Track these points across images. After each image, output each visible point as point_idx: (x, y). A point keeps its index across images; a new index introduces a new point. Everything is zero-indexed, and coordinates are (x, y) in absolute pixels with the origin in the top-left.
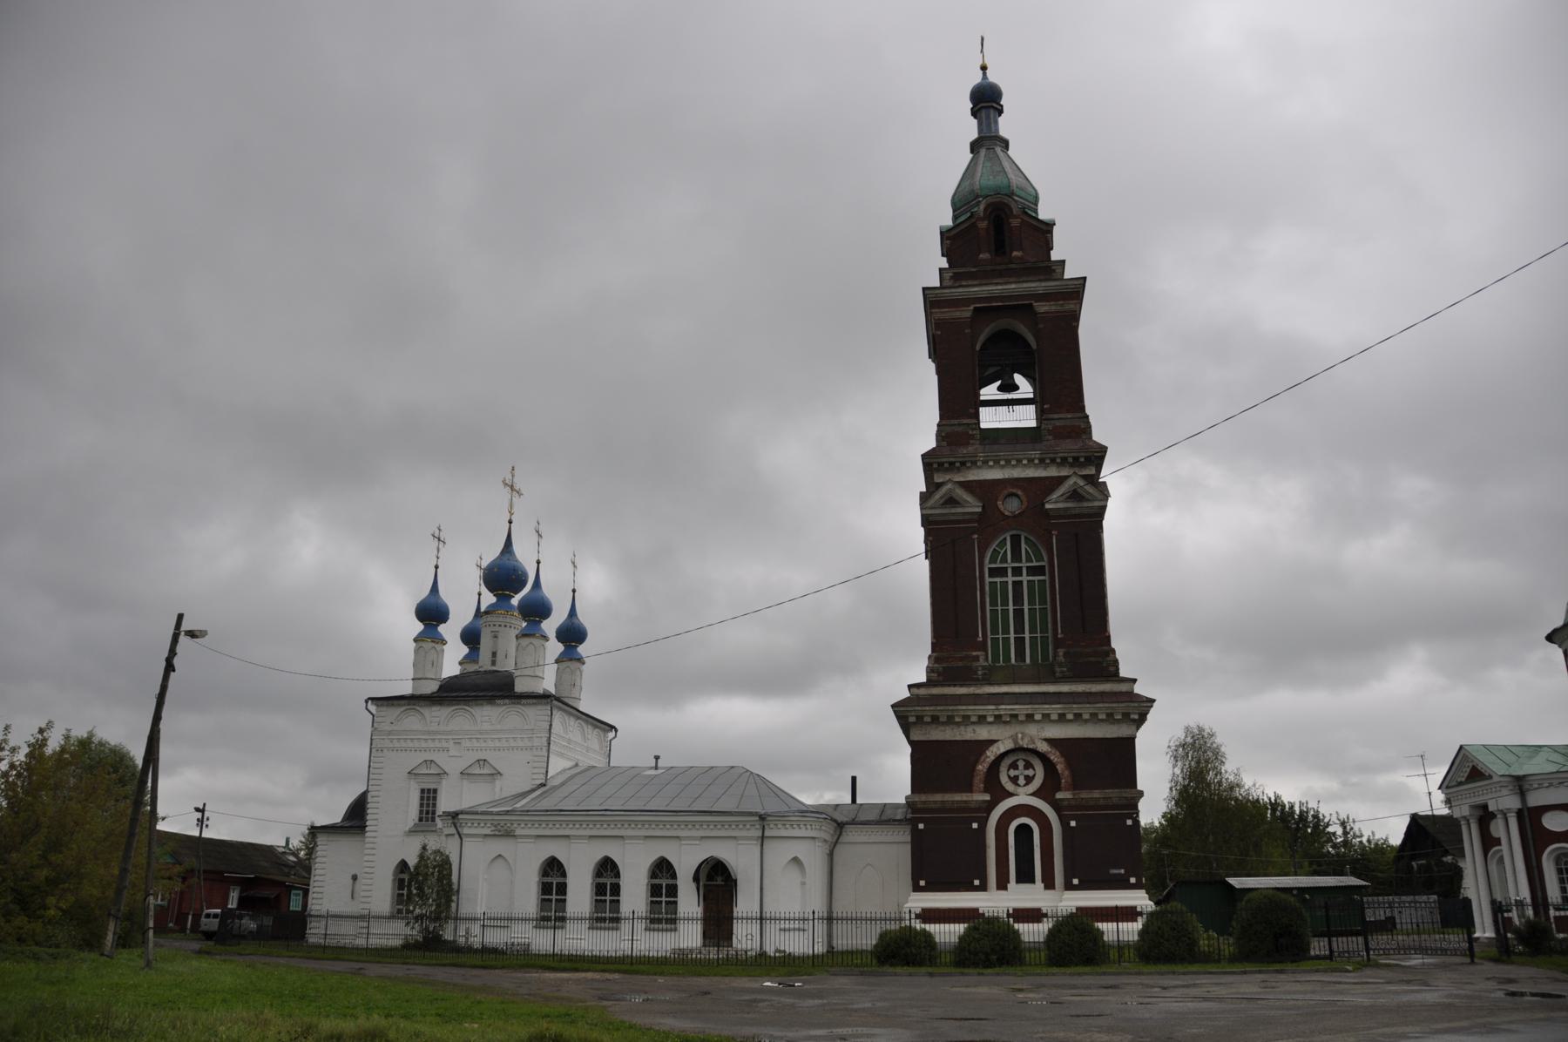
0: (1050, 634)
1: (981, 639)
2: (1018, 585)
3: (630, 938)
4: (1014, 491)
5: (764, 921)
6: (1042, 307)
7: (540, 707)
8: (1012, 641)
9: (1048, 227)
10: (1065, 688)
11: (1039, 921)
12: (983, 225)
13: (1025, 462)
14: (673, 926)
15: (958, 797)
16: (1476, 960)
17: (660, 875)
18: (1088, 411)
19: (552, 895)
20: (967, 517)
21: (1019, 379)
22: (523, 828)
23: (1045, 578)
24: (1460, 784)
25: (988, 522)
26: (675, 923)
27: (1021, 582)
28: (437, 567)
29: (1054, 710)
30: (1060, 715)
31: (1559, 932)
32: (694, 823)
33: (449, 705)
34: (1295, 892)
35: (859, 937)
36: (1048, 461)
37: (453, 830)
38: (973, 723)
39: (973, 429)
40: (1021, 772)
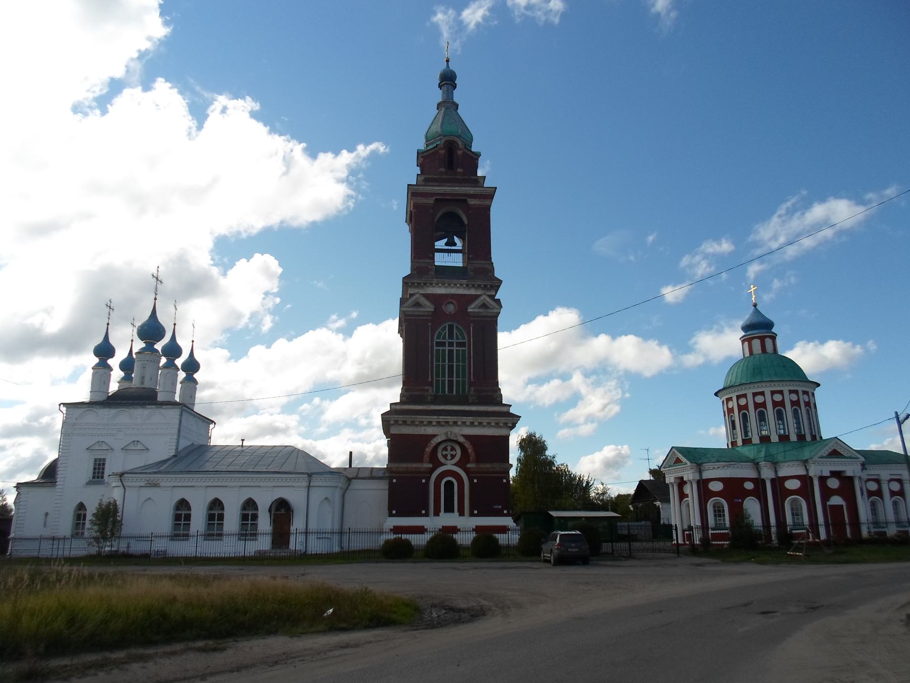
2: (451, 352)
3: (195, 545)
4: (452, 301)
5: (308, 534)
8: (447, 381)
12: (443, 152)
13: (458, 285)
14: (254, 538)
15: (415, 465)
16: (680, 555)
17: (248, 508)
19: (181, 521)
20: (426, 314)
21: (456, 239)
22: (216, 482)
23: (466, 349)
24: (670, 466)
25: (438, 316)
26: (256, 536)
27: (453, 350)
28: (108, 324)
29: (469, 420)
30: (504, 423)
31: (687, 541)
33: (115, 408)
34: (583, 519)
36: (470, 286)
37: (120, 484)
38: (425, 425)
39: (431, 266)
40: (449, 453)
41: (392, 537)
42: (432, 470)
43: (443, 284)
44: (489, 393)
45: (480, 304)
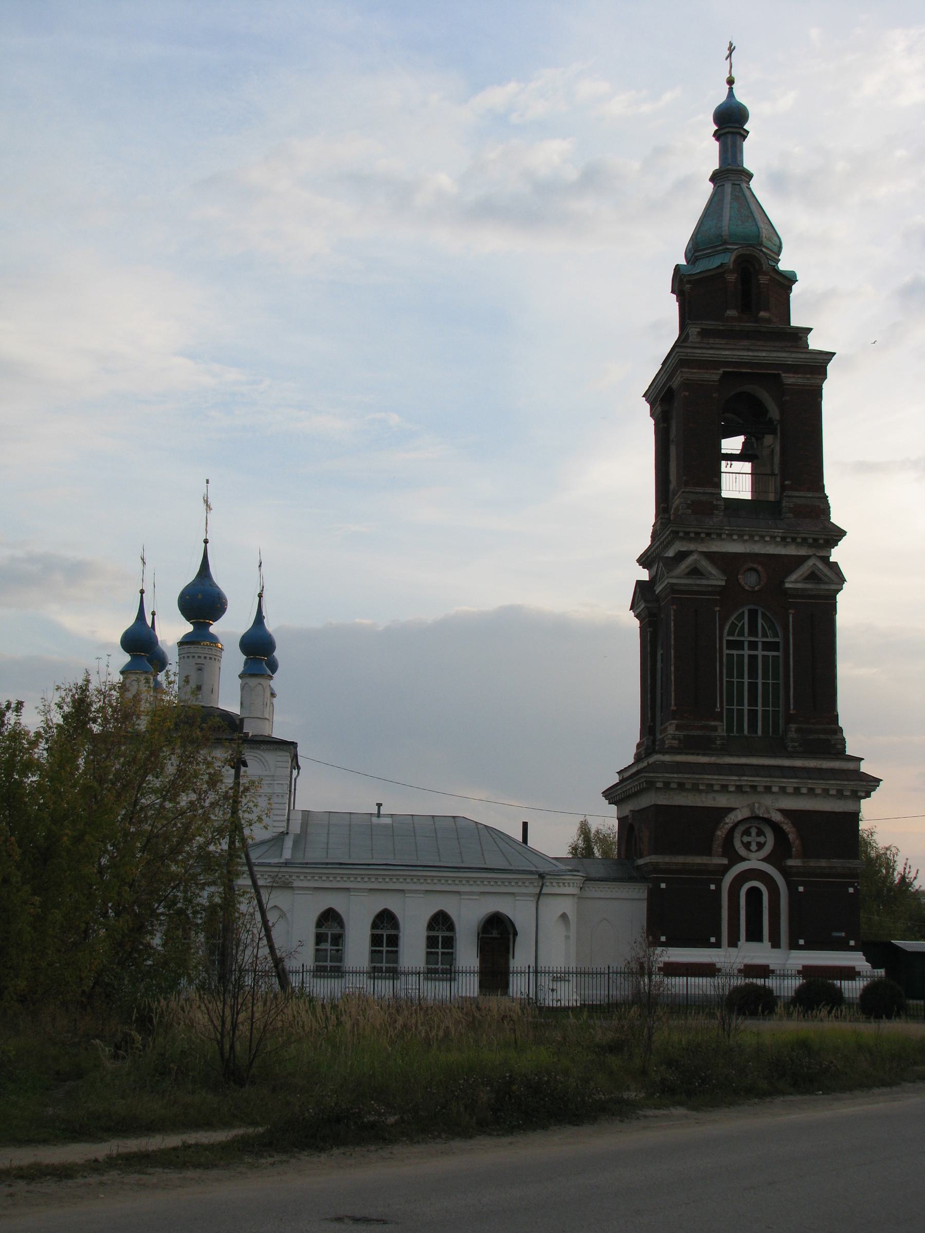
0: (781, 709)
1: (719, 710)
2: (753, 658)
4: (755, 566)
5: (539, 974)
6: (789, 379)
7: (280, 753)
9: (789, 280)
10: (798, 763)
11: (853, 979)
13: (767, 539)
18: (827, 492)
20: (710, 589)
27: (757, 656)
29: (791, 783)
32: (475, 880)
35: (587, 987)
36: (789, 540)
38: (715, 791)
40: (753, 839)
41: (740, 982)
42: (725, 869)
43: (741, 536)
44: (822, 736)
45: (806, 574)
